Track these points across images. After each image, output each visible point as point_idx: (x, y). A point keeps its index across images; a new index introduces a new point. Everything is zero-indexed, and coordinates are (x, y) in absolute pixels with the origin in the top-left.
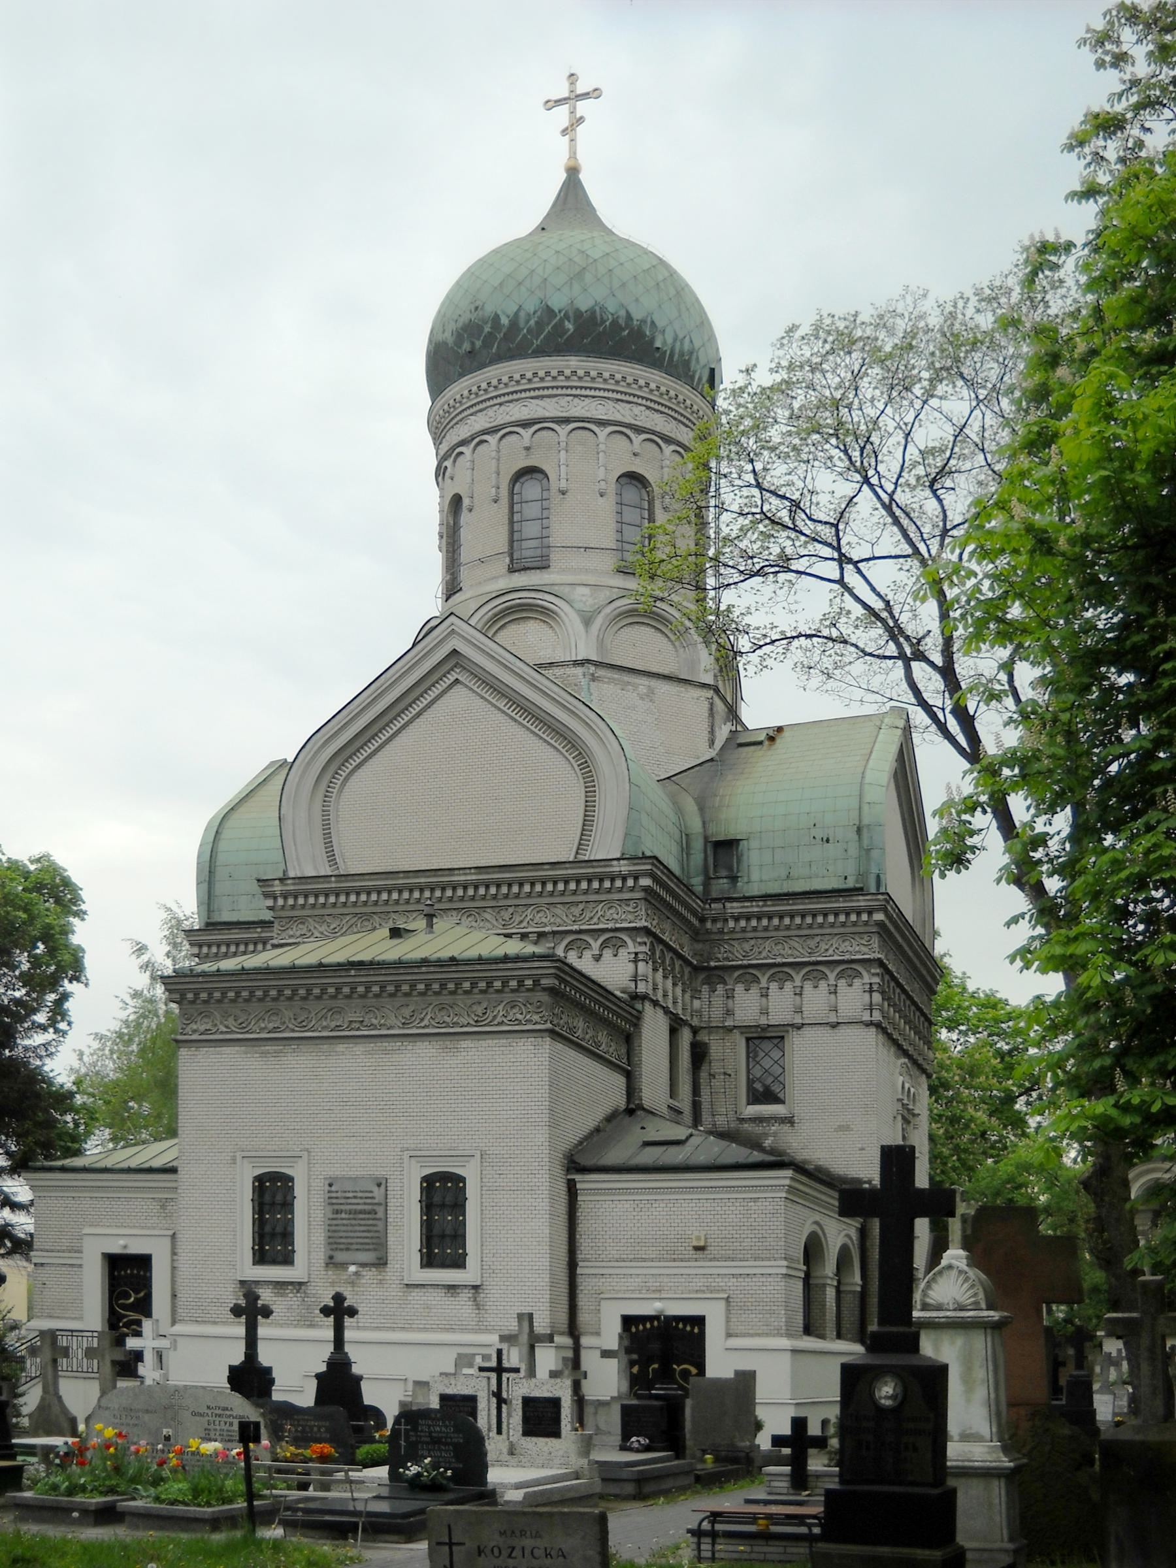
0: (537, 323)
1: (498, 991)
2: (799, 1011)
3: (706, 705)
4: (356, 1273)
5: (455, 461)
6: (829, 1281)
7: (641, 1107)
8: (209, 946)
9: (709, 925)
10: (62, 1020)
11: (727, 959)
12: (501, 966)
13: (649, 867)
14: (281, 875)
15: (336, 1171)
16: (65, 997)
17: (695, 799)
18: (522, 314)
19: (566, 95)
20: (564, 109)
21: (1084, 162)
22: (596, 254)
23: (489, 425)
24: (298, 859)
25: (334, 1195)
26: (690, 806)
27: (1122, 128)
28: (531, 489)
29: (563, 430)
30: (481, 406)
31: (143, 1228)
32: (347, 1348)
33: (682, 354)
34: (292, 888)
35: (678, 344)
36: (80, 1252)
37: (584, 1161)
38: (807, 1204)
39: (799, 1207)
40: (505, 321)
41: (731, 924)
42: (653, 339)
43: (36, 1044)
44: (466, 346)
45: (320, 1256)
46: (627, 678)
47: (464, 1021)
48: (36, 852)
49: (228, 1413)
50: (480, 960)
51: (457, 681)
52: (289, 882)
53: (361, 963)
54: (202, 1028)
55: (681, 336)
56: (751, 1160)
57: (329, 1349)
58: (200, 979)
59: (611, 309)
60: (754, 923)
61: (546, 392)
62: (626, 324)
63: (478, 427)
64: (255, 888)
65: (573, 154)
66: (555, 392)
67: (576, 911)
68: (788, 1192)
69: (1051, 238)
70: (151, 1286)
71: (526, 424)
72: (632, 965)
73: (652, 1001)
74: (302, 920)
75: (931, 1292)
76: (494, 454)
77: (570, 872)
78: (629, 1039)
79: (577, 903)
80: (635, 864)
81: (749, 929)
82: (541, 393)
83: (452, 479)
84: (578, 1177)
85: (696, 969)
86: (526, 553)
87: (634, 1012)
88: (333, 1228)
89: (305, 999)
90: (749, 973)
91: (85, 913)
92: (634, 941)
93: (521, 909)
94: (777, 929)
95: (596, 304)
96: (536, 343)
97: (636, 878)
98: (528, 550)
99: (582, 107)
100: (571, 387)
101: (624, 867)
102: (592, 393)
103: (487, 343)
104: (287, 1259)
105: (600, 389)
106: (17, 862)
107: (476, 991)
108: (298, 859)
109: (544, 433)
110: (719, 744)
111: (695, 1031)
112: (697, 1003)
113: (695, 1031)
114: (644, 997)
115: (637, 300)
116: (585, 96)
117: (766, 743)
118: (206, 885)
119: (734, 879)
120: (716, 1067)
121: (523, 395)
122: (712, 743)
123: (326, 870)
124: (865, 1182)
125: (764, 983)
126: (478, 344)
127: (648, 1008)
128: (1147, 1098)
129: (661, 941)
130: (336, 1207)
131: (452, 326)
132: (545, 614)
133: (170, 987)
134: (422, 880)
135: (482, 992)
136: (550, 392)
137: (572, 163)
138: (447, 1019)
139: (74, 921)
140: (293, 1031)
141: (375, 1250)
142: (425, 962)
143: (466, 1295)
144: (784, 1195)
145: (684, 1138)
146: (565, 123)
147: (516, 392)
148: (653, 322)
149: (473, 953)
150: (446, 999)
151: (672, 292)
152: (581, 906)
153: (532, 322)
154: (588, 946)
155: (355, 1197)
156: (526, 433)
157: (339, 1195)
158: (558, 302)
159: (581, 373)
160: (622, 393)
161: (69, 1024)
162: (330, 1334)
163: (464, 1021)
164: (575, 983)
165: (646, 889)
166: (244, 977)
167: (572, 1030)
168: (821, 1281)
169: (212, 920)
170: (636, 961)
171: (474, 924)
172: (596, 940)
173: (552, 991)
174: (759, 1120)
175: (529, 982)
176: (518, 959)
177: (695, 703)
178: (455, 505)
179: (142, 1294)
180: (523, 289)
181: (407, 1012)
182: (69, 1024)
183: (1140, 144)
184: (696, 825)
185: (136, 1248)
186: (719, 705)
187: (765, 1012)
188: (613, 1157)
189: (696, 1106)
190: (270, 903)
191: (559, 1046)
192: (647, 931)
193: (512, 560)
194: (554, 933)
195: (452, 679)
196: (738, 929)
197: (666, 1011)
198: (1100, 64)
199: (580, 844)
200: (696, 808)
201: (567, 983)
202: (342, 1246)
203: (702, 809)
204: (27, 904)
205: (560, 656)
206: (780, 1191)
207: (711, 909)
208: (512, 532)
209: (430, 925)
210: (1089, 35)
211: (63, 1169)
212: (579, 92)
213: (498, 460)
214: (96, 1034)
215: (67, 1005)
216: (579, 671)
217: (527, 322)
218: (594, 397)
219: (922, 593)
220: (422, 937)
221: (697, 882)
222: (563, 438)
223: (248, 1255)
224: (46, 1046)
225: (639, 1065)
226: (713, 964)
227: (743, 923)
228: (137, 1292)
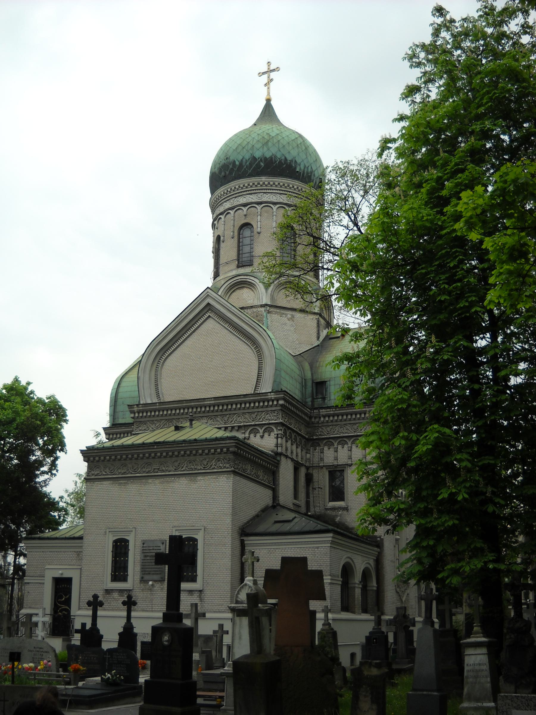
0: (250, 163)
1: (213, 454)
2: (350, 458)
3: (316, 321)
4: (152, 585)
5: (218, 222)
6: (357, 586)
7: (279, 505)
8: (113, 435)
9: (313, 420)
10: (55, 469)
11: (321, 435)
12: (214, 443)
13: (283, 396)
14: (137, 403)
15: (146, 538)
16: (56, 458)
17: (309, 363)
18: (244, 160)
19: (266, 70)
20: (266, 76)
21: (408, 104)
22: (273, 134)
23: (231, 206)
24: (144, 396)
25: (144, 548)
26: (307, 366)
27: (420, 91)
28: (247, 232)
29: (259, 207)
30: (228, 198)
31: (70, 565)
32: (132, 621)
33: (308, 173)
34: (141, 408)
35: (306, 170)
36: (44, 577)
37: (248, 531)
38: (343, 549)
39: (339, 551)
40: (237, 163)
41: (322, 419)
42: (296, 168)
43: (40, 481)
44: (223, 174)
45: (138, 578)
46: (282, 311)
47: (199, 468)
48: (49, 394)
49: (41, 650)
50: (206, 440)
51: (209, 316)
52: (140, 406)
53: (159, 442)
54: (96, 473)
55: (307, 166)
56: (317, 529)
57: (124, 621)
58: (96, 451)
59: (279, 157)
60: (331, 418)
61: (253, 192)
62: (285, 162)
63: (227, 207)
64: (127, 409)
65: (269, 93)
66: (256, 191)
67: (254, 416)
68: (331, 543)
69: (388, 137)
70: (71, 593)
71: (245, 205)
72: (275, 440)
73: (284, 455)
74: (145, 423)
75: (239, 596)
76: (232, 218)
77: (251, 398)
78: (274, 473)
79: (254, 412)
80: (277, 395)
81: (329, 421)
82: (251, 192)
83: (217, 228)
84: (245, 538)
85: (308, 440)
86: (244, 259)
87: (276, 461)
88: (144, 564)
89: (137, 459)
90: (329, 442)
91: (68, 421)
92: (277, 429)
93: (231, 416)
94: (341, 421)
95: (273, 155)
96: (250, 171)
97: (278, 401)
98: (245, 258)
99: (273, 75)
100: (263, 189)
101: (273, 396)
102: (271, 191)
103: (231, 173)
104: (124, 579)
105: (274, 189)
106: (41, 398)
107: (204, 454)
108: (144, 396)
109: (252, 209)
110: (321, 339)
111: (308, 468)
112: (308, 456)
113: (308, 468)
114: (281, 454)
115: (289, 152)
116: (274, 70)
117: (341, 337)
118: (113, 407)
119: (324, 399)
120: (316, 485)
121: (244, 193)
122: (318, 338)
123: (155, 400)
124: (378, 537)
125: (336, 446)
126: (227, 173)
127: (283, 459)
128: (393, 505)
129: (289, 428)
130: (145, 554)
131: (218, 166)
132: (250, 285)
133: (85, 455)
134: (193, 404)
135: (207, 454)
136: (255, 191)
137: (268, 97)
138: (192, 467)
139: (64, 424)
140: (132, 473)
141: (160, 574)
142: (184, 441)
143: (196, 595)
144: (329, 545)
145: (291, 519)
146: (266, 81)
147: (241, 192)
148: (295, 161)
149: (204, 437)
150: (192, 458)
151: (304, 148)
152: (256, 414)
153: (248, 163)
154: (258, 432)
155: (153, 549)
156: (245, 209)
157: (147, 548)
158: (258, 155)
159: (266, 183)
160: (283, 190)
161: (57, 471)
162: (125, 614)
163: (199, 468)
164: (247, 450)
165: (282, 405)
166: (113, 450)
167: (244, 470)
168: (353, 586)
169: (114, 423)
170: (277, 438)
171: (213, 423)
172: (261, 429)
173: (234, 453)
174: (334, 509)
175: (225, 450)
176: (222, 439)
177: (311, 321)
178: (218, 240)
179: (68, 596)
180: (244, 150)
181: (176, 464)
182: (57, 471)
183: (428, 96)
184: (309, 375)
185: (67, 575)
186: (322, 321)
187: (336, 459)
188: (261, 528)
189: (308, 503)
190: (132, 415)
191: (238, 478)
192: (282, 424)
193: (239, 263)
194: (245, 426)
195: (208, 315)
196: (325, 421)
197: (292, 460)
198: (411, 66)
199: (256, 386)
200: (309, 367)
201: (241, 449)
202: (147, 572)
203: (311, 368)
204: (42, 418)
205: (256, 303)
206: (327, 543)
207: (314, 413)
208: (239, 250)
209: (191, 424)
210: (406, 56)
211: (40, 538)
212: (271, 69)
213: (234, 220)
214: (78, 474)
215: (57, 462)
216: (263, 309)
217: (246, 163)
218: (271, 193)
219: (328, 286)
220: (188, 430)
221: (309, 400)
222: (259, 210)
223: (109, 577)
224: (45, 481)
225: (278, 485)
226: (315, 437)
227: (327, 419)
228: (66, 596)
